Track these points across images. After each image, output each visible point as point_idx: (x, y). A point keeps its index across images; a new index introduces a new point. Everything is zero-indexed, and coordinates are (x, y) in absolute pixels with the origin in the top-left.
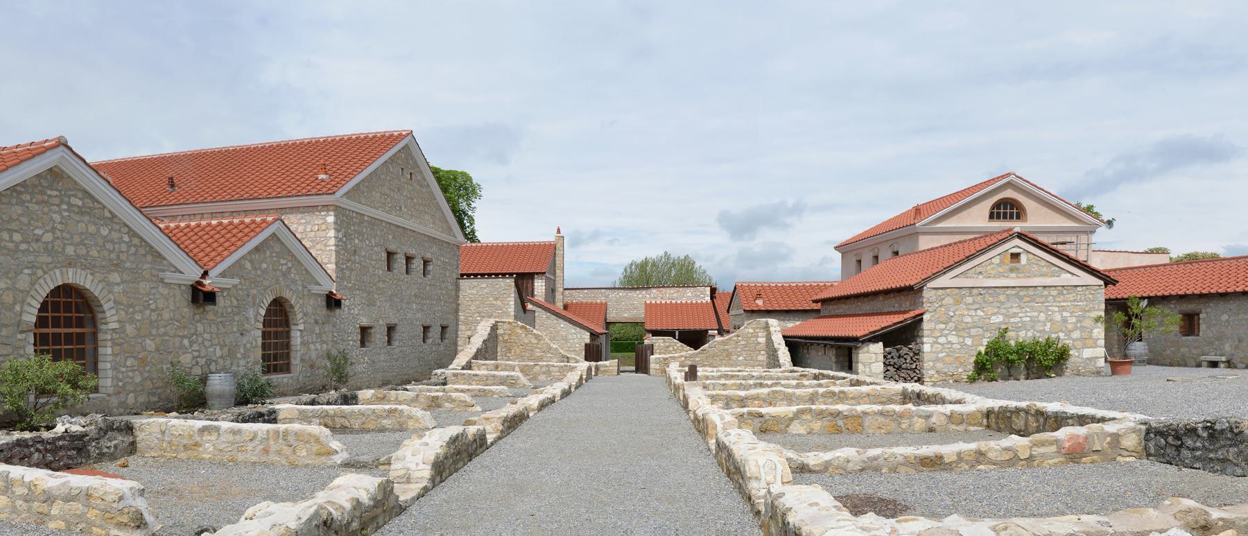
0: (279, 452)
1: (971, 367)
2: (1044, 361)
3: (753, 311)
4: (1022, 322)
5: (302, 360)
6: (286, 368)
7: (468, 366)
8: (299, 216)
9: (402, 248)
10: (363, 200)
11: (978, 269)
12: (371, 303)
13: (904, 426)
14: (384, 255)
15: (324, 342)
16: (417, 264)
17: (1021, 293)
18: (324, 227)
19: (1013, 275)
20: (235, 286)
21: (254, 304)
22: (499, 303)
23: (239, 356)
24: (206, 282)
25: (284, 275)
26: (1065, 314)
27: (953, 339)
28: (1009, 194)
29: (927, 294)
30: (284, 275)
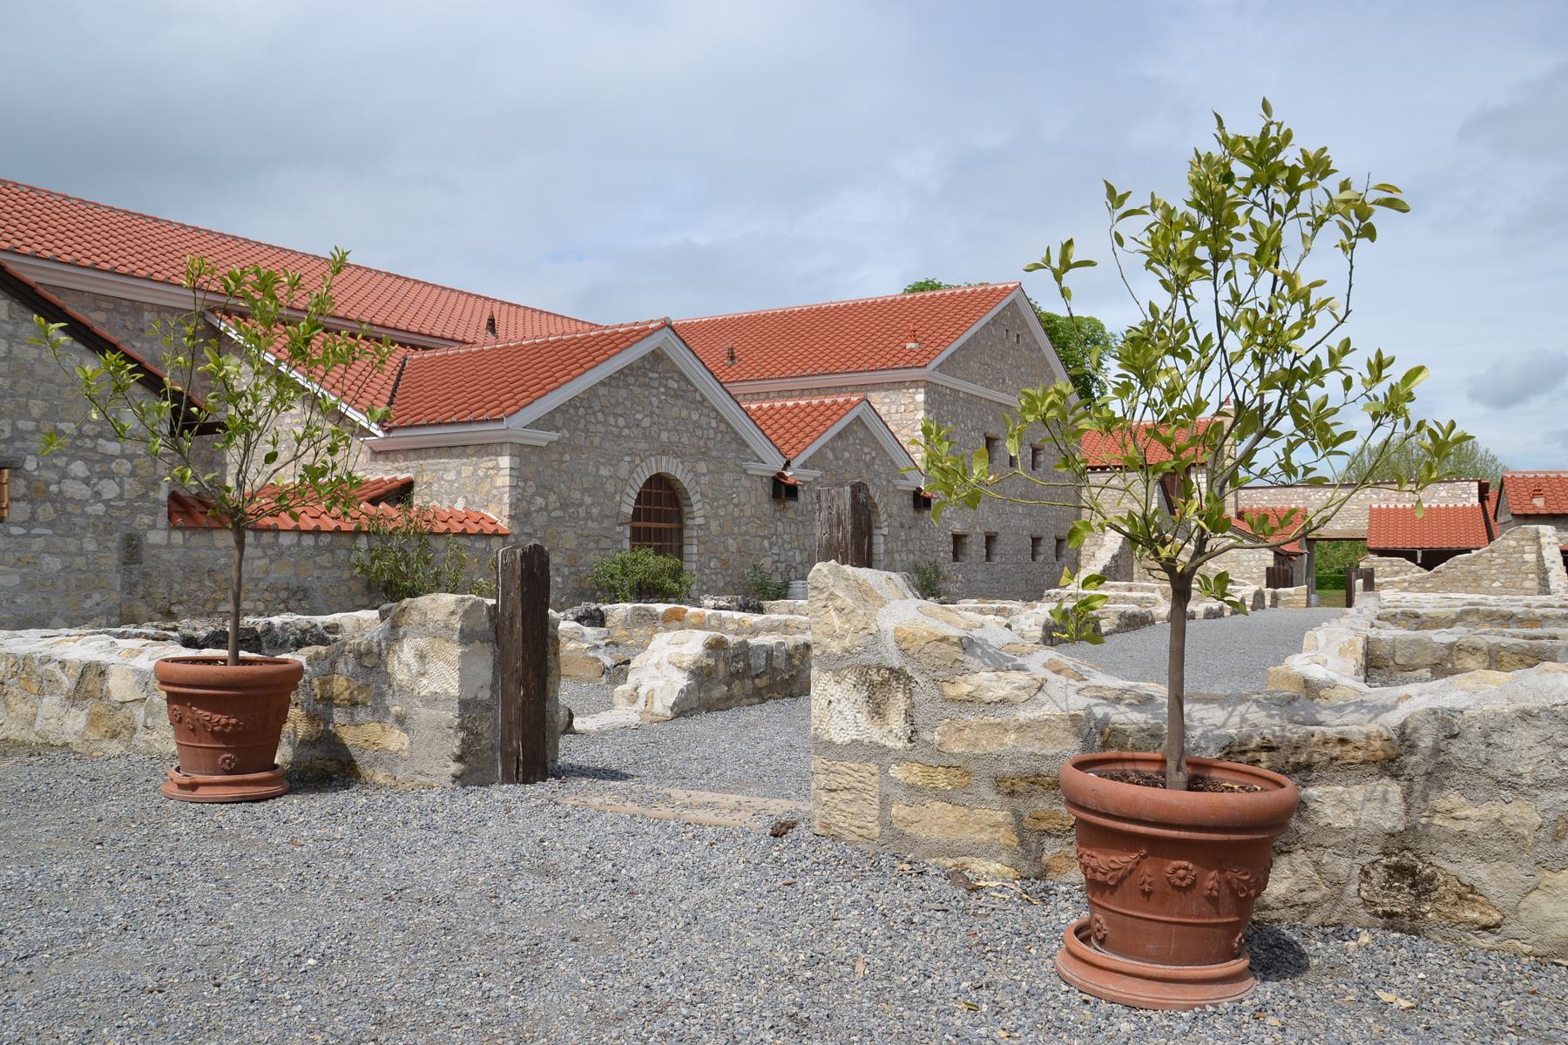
8: (883, 394)
10: (959, 373)
14: (983, 441)
18: (912, 407)
24: (788, 474)
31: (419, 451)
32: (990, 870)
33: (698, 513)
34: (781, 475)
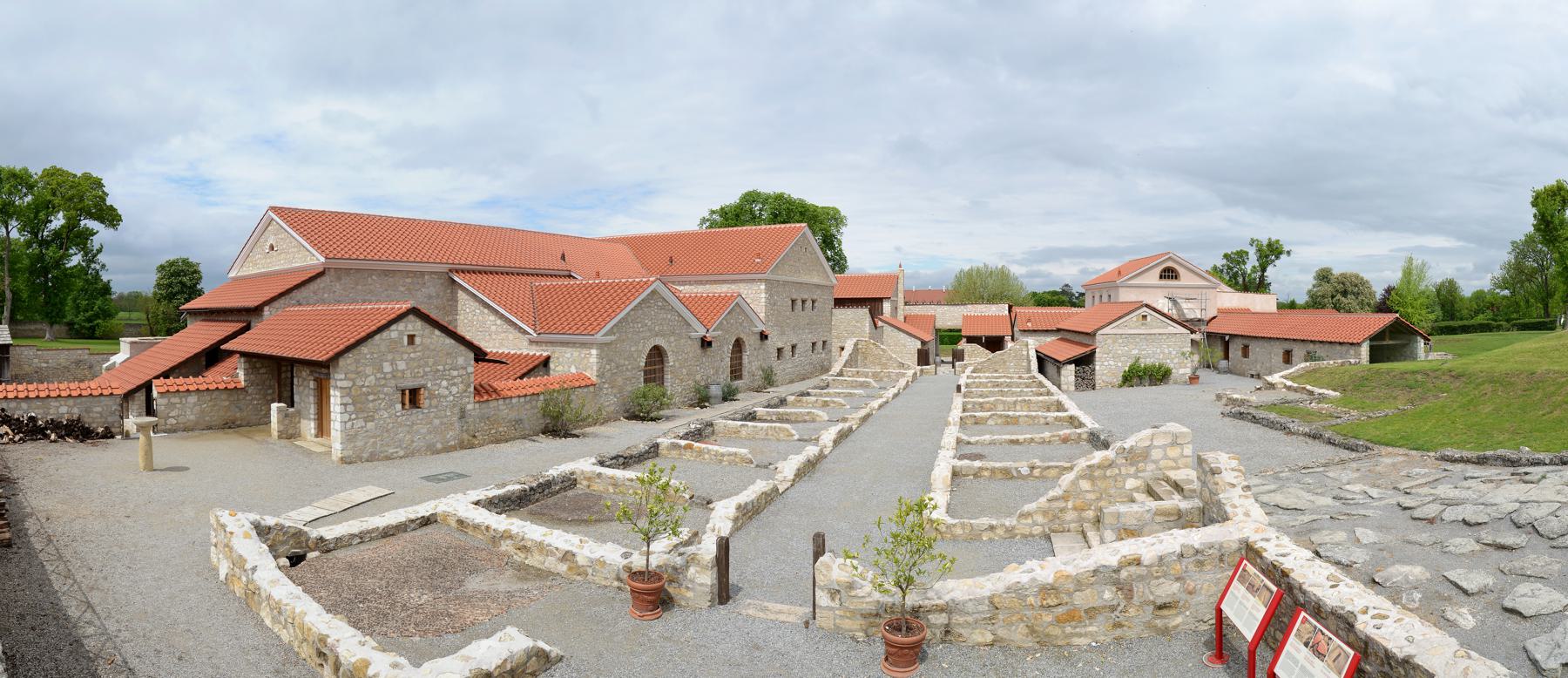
2: (1159, 376)
6: (740, 377)
7: (840, 374)
9: (798, 296)
12: (783, 333)
16: (809, 304)
28: (1170, 264)
29: (1098, 337)
31: (552, 343)
32: (860, 635)
33: (671, 360)
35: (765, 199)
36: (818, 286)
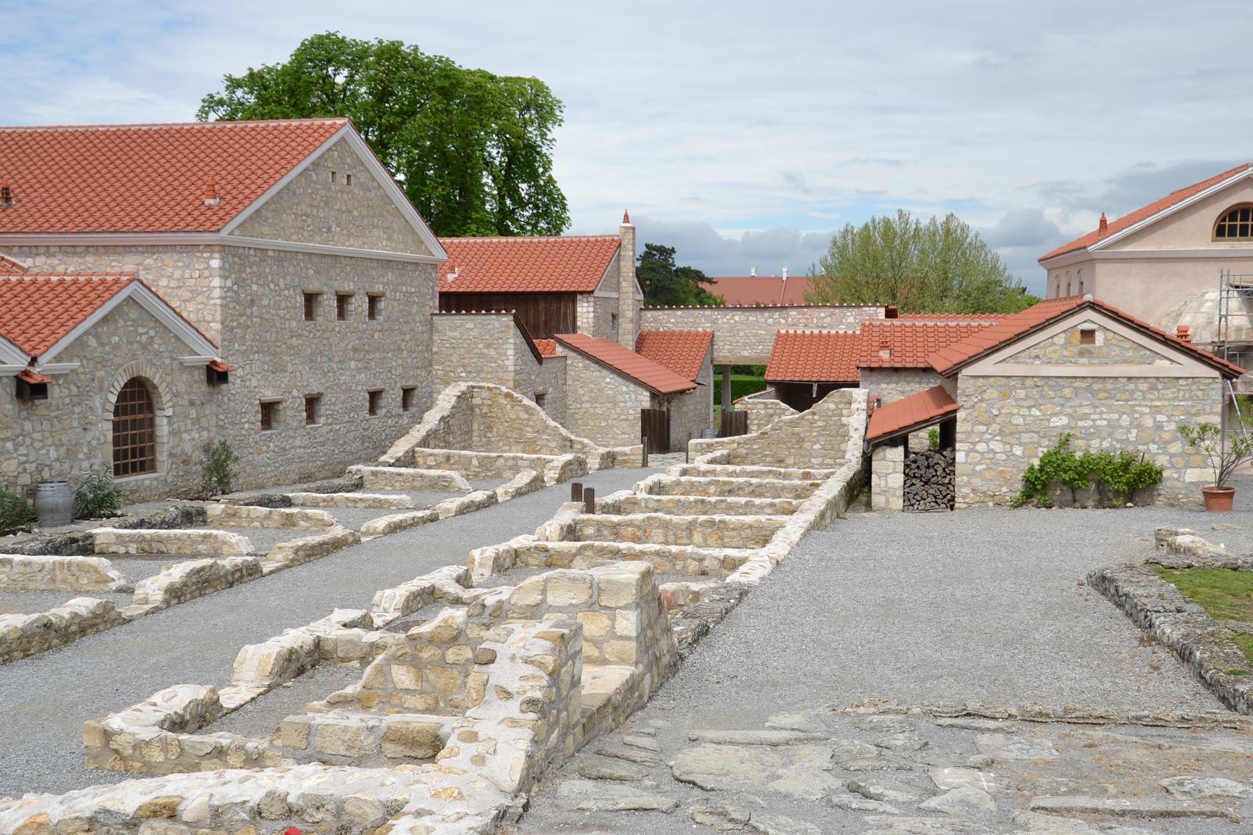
0: (64, 581)
1: (1019, 486)
3: (871, 369)
4: (1095, 427)
5: (171, 455)
7: (409, 460)
8: (175, 257)
10: (266, 230)
11: (1034, 352)
12: (278, 369)
13: (678, 567)
14: (301, 300)
15: (203, 429)
17: (1095, 387)
18: (206, 273)
19: (1084, 360)
20: (73, 371)
21: (101, 390)
22: (492, 352)
23: (81, 456)
24: (35, 370)
25: (144, 347)
26: (1159, 417)
27: (996, 446)
30: (144, 347)
34: (26, 373)
35: (355, 56)
36: (387, 263)
